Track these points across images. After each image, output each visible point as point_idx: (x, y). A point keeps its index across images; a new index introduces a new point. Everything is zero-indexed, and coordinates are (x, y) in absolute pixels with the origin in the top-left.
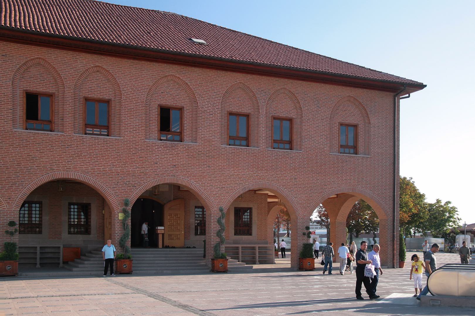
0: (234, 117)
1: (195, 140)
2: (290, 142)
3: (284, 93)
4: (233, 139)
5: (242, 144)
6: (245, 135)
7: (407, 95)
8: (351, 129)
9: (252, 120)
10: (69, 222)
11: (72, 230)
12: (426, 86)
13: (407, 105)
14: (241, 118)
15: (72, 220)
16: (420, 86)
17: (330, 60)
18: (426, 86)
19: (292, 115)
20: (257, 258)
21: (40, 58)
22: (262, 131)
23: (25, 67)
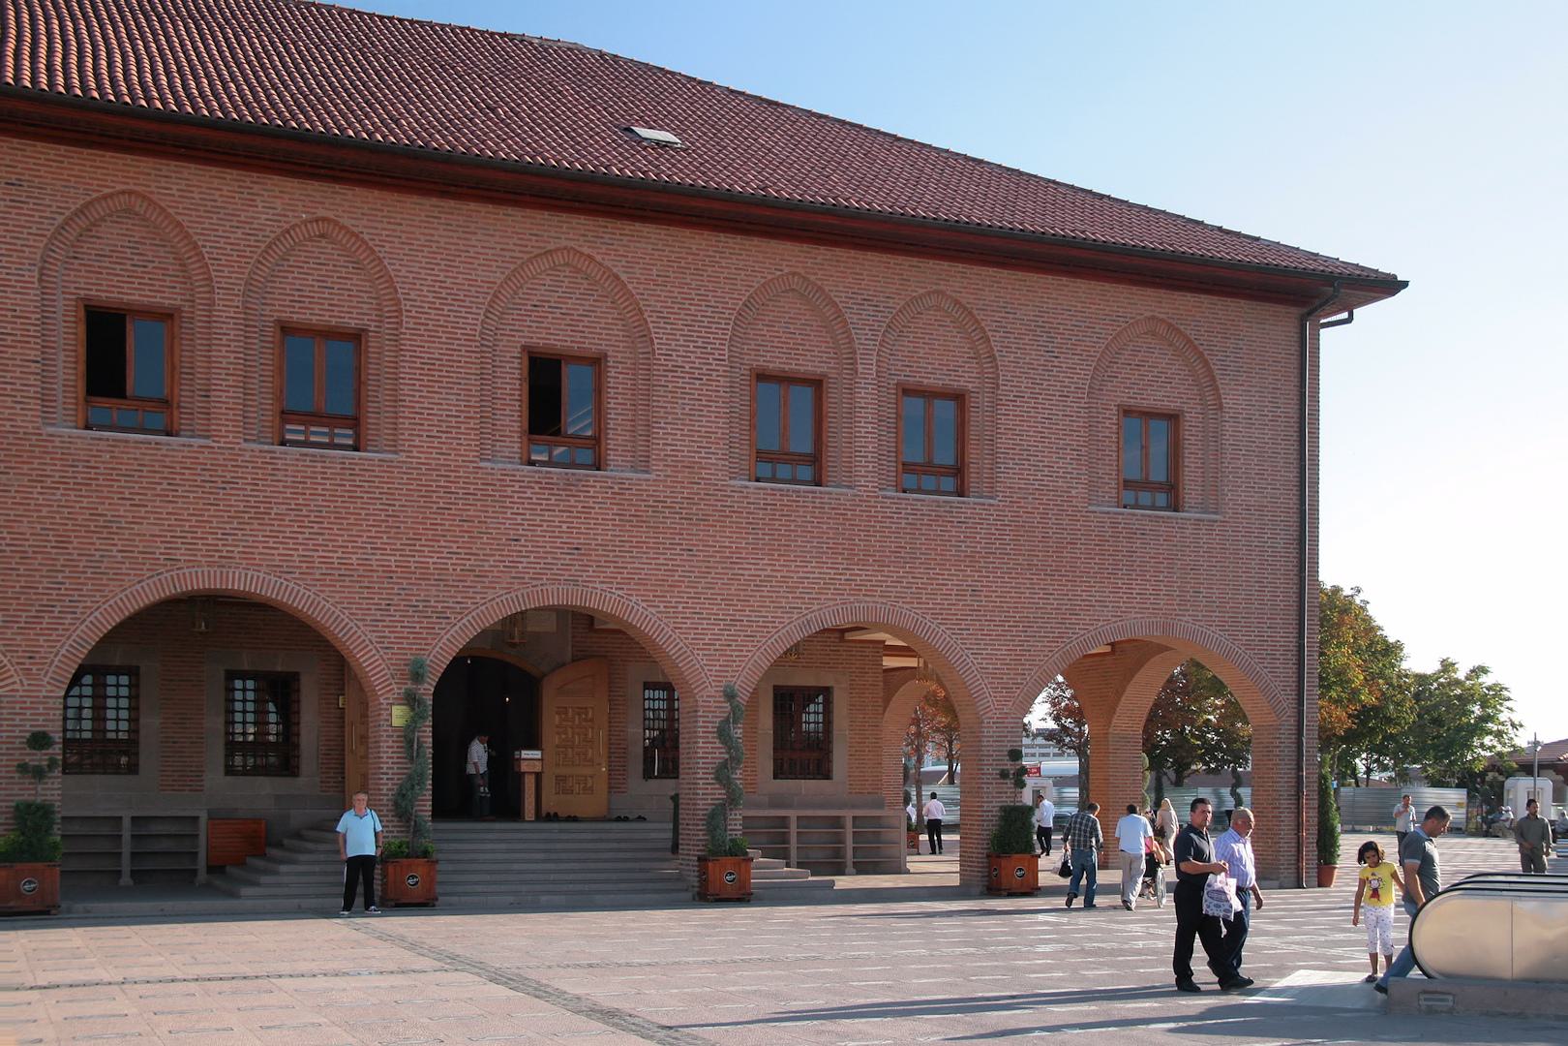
0: (773, 388)
1: (643, 464)
2: (958, 471)
3: (938, 309)
4: (770, 462)
5: (800, 477)
6: (807, 447)
7: (1345, 315)
8: (1160, 427)
9: (833, 397)
10: (227, 733)
11: (238, 760)
12: (1405, 284)
13: (1343, 348)
14: (795, 389)
15: (239, 729)
16: (1387, 286)
17: (1089, 198)
18: (1405, 284)
19: (965, 379)
20: (850, 853)
21: (131, 193)
22: (864, 433)
23: (83, 222)
